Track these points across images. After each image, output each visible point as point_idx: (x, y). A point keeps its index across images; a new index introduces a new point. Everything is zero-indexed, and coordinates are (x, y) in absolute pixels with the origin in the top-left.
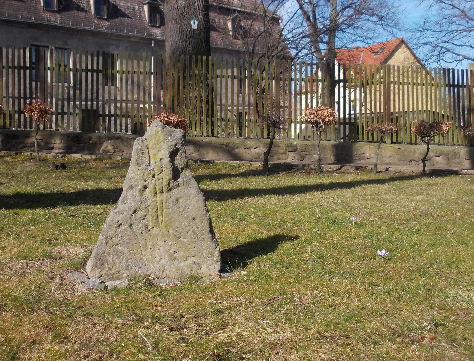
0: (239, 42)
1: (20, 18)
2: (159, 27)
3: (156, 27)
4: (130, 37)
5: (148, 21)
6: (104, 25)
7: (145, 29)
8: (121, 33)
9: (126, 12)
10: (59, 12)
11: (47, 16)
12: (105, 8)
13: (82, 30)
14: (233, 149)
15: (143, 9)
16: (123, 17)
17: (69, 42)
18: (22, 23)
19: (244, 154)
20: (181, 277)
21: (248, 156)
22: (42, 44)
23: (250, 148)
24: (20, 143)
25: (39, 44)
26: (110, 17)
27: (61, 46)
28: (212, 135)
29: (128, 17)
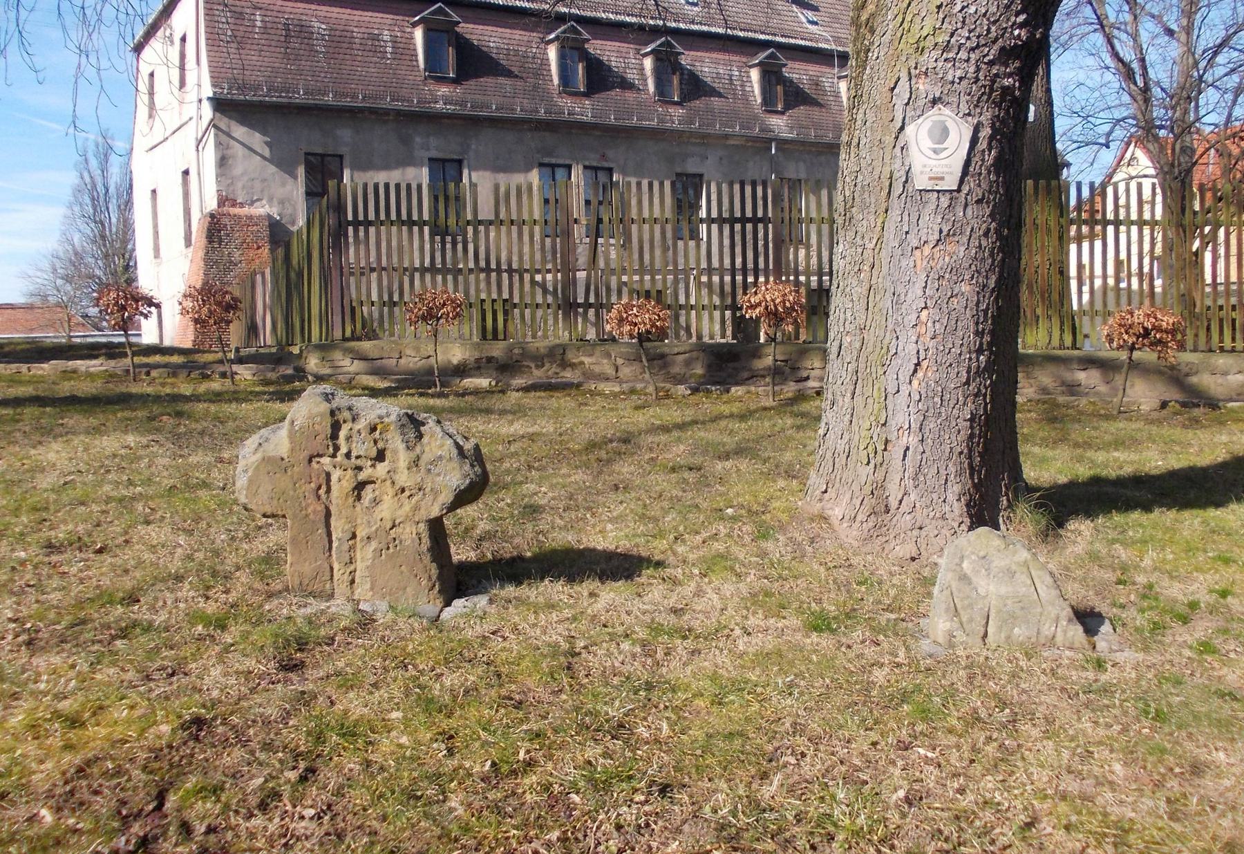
0: (677, 113)
1: (518, 113)
2: (783, 113)
3: (777, 112)
4: (727, 136)
5: (759, 101)
6: (780, 124)
7: (756, 117)
8: (627, 123)
9: (716, 85)
10: (587, 95)
11: (566, 103)
12: (676, 80)
13: (636, 129)
14: (1187, 375)
15: (749, 77)
16: (711, 96)
17: (610, 154)
18: (523, 121)
19: (1212, 386)
20: (1010, 619)
21: (1220, 389)
22: (561, 161)
23: (1225, 374)
24: (744, 368)
25: (553, 161)
26: (685, 98)
27: (595, 164)
28: (1074, 346)
29: (720, 95)
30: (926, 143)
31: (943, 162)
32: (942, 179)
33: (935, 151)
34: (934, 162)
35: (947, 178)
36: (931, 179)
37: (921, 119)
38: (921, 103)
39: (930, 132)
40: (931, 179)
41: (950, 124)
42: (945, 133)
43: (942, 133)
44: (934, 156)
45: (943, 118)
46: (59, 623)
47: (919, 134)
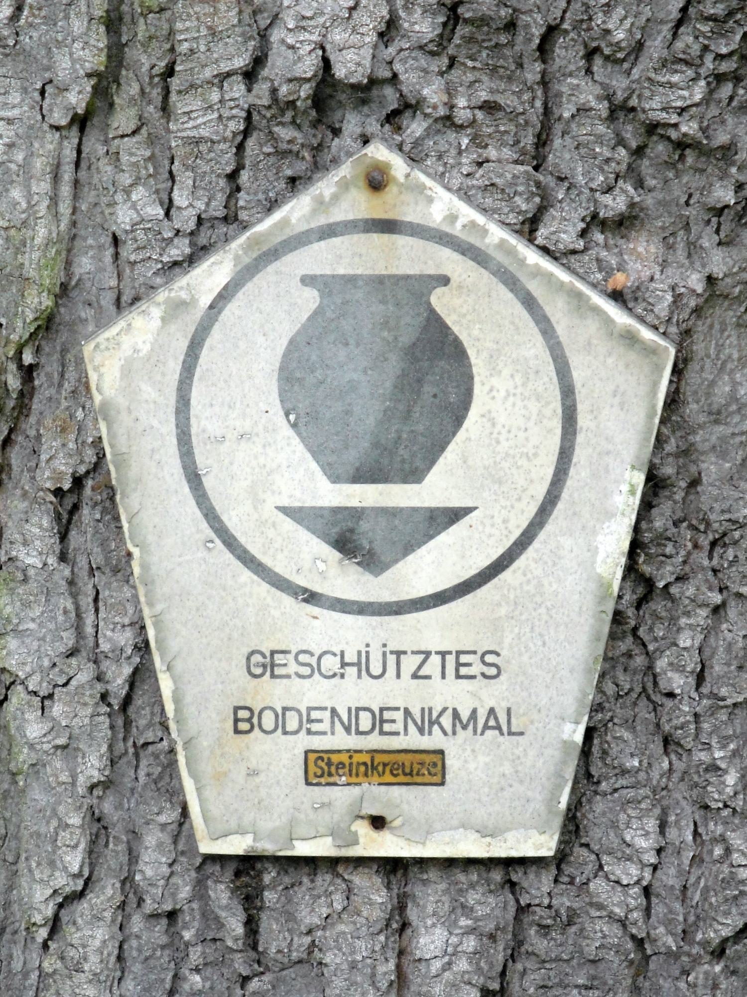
30: (275, 473)
31: (432, 630)
32: (422, 769)
33: (348, 537)
34: (351, 634)
35: (464, 756)
36: (322, 768)
37: (212, 275)
38: (202, 118)
39: (296, 375)
40: (322, 768)
41: (475, 311)
42: (430, 378)
43: (405, 389)
44: (346, 581)
45: (407, 257)
46: (48, 461)
47: (206, 394)
